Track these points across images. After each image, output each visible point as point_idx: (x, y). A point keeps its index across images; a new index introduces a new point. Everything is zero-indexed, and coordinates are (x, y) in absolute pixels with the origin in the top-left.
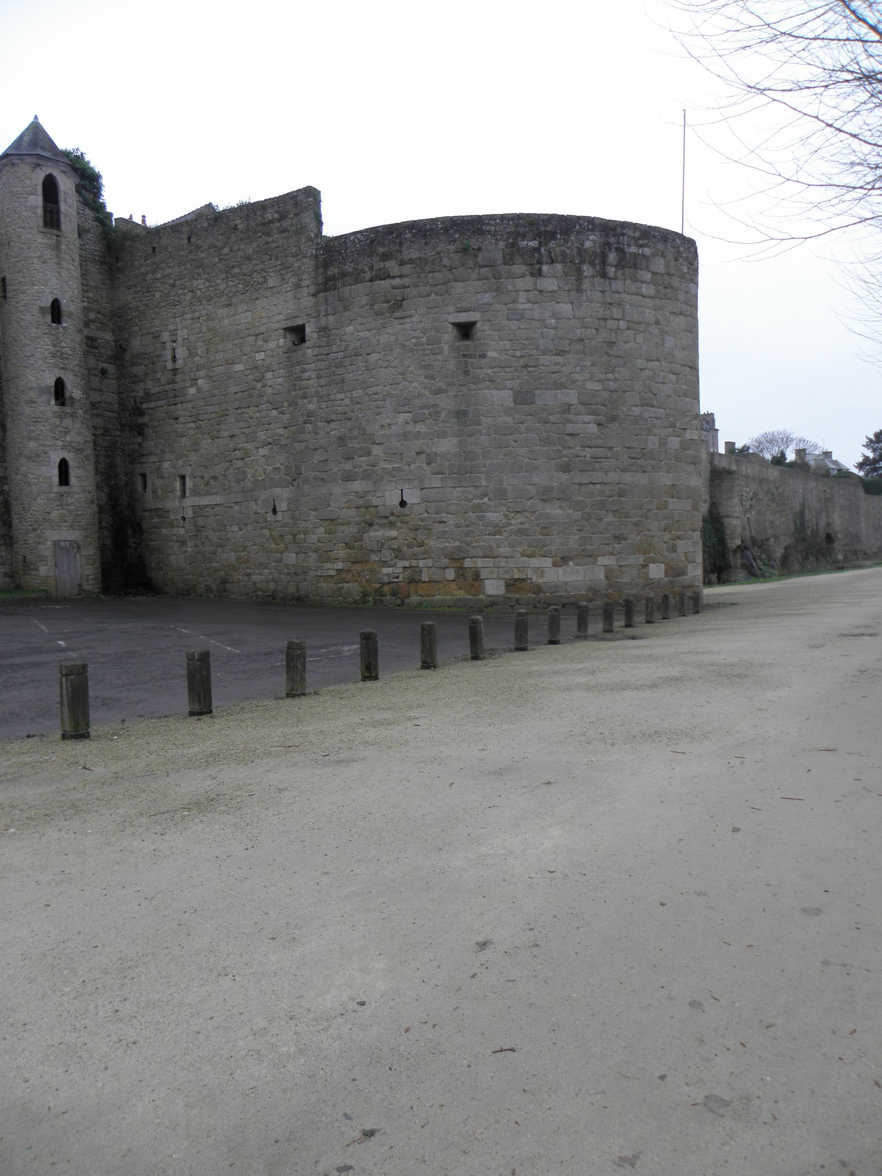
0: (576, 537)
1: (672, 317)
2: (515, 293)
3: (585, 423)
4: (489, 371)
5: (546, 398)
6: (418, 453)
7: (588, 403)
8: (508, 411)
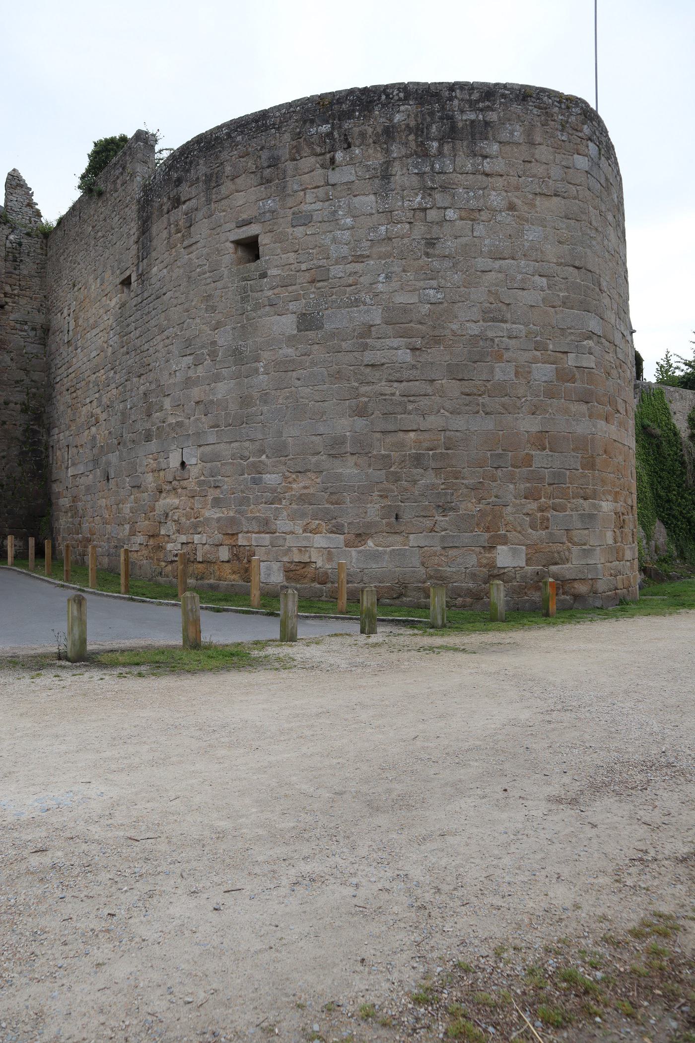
0: (377, 506)
1: (538, 201)
2: (302, 193)
3: (392, 348)
4: (270, 293)
5: (338, 320)
6: (197, 403)
7: (398, 320)
8: (291, 340)
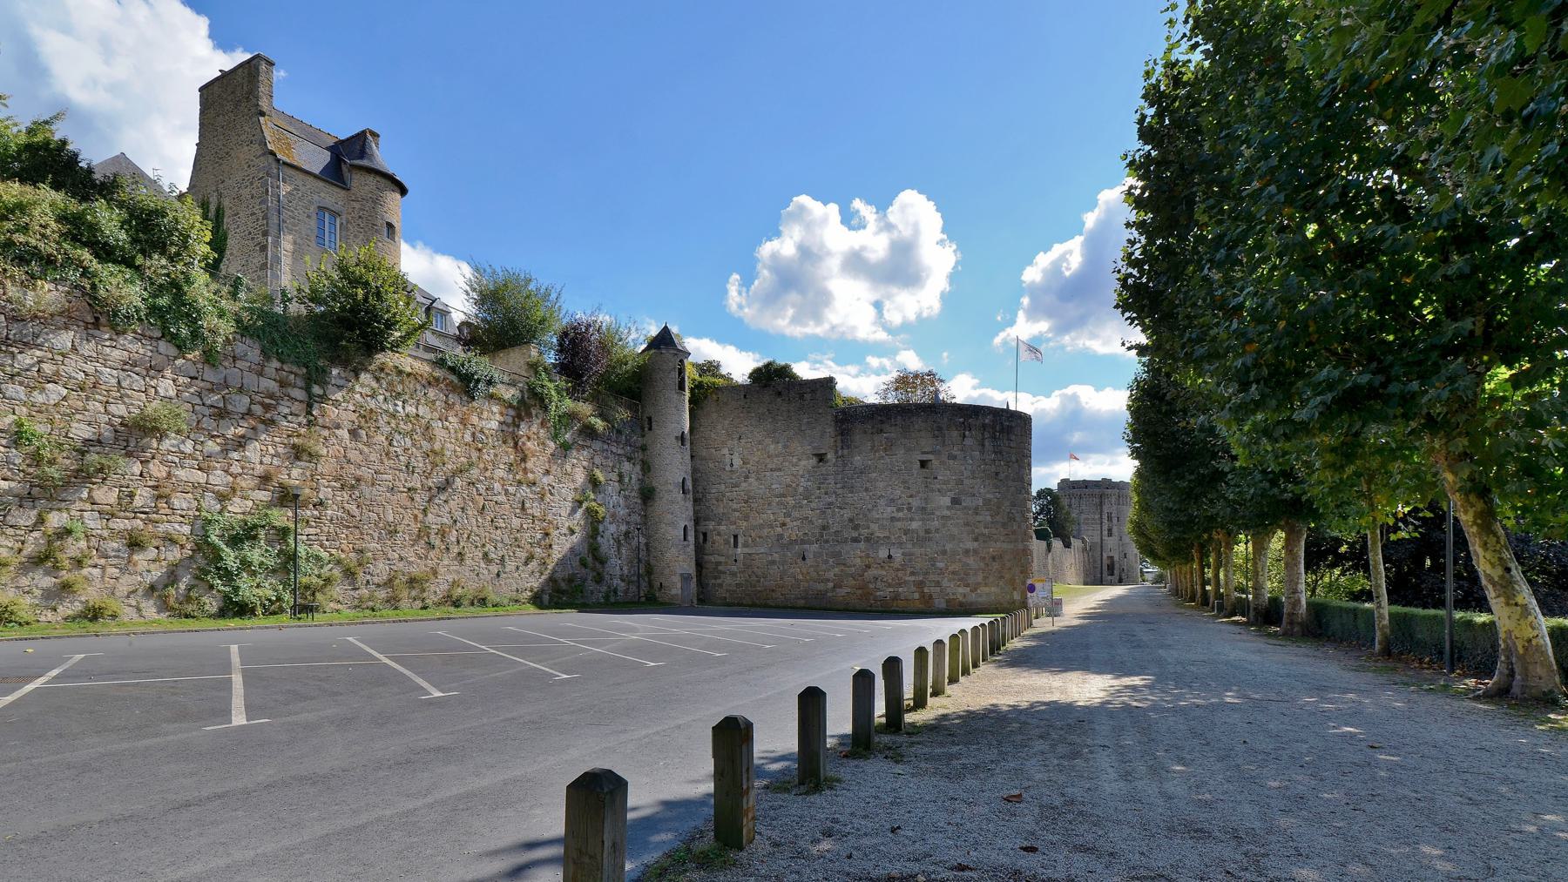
5: (967, 502)
8: (948, 508)
